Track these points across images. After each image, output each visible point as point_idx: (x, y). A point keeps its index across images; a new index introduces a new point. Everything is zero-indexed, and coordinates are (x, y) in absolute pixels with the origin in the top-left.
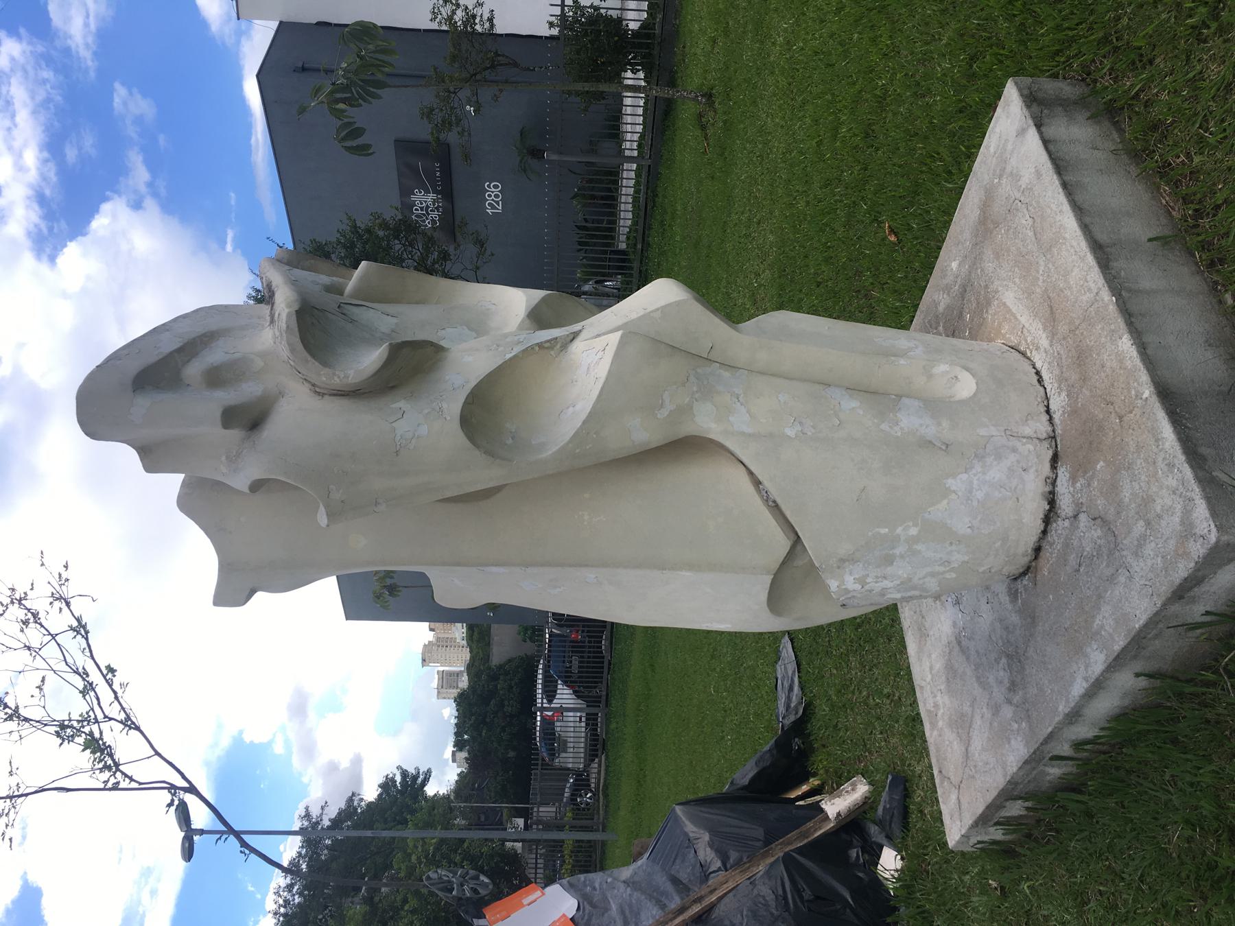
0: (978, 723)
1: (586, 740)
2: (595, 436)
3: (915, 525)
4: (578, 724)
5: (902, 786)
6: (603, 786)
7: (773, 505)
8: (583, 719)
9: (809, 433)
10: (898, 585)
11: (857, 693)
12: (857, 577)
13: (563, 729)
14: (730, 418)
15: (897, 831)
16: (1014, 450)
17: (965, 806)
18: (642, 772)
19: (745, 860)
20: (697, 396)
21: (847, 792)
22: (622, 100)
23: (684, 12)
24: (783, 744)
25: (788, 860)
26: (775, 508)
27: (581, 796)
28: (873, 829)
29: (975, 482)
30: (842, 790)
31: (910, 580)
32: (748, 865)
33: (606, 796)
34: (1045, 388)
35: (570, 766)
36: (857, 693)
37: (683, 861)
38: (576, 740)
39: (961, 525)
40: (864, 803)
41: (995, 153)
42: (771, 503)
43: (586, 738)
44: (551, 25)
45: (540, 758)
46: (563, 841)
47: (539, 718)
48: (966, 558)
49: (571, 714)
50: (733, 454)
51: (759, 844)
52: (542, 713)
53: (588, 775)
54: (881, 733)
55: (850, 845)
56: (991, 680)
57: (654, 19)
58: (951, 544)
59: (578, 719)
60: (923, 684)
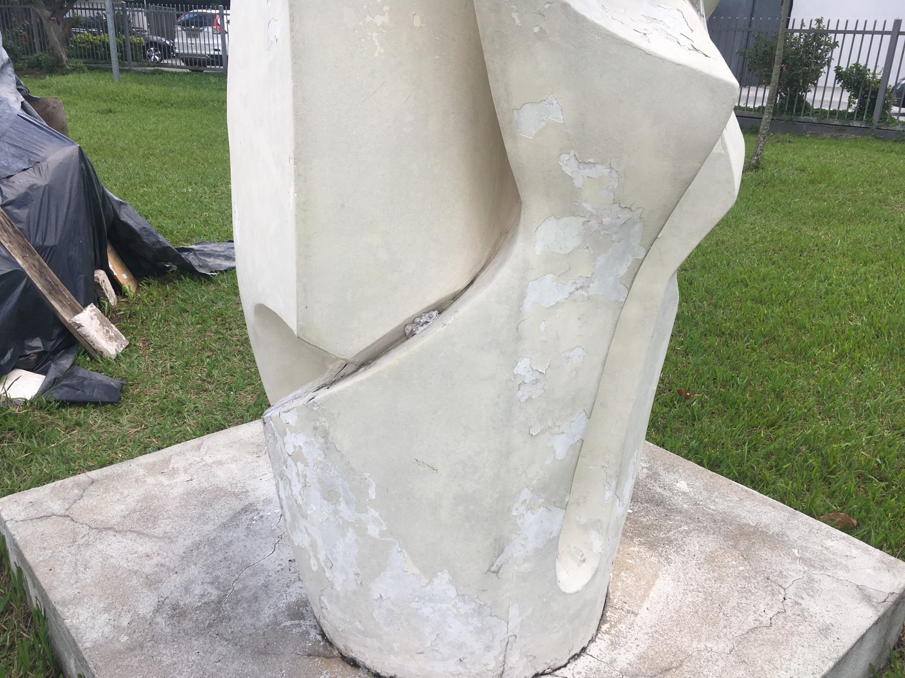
0: (141, 549)
1: (199, 55)
2: (536, 30)
3: (382, 534)
4: (212, 48)
5: (107, 399)
6: (162, 70)
7: (407, 332)
8: (216, 53)
9: (519, 394)
10: (296, 501)
11: (216, 337)
12: (303, 451)
13: (206, 34)
14: (550, 277)
15: (58, 394)
16: (488, 648)
17: (42, 527)
18: (170, 105)
19: (17, 226)
20: (594, 223)
21: (108, 331)
22: (755, 85)
23: (817, 141)
24: (165, 253)
25: (18, 275)
26: (403, 335)
27: (156, 51)
28: (66, 362)
29: (444, 606)
30: (109, 326)
31: (305, 517)
32: (11, 230)
33: (154, 73)
34: (565, 666)
35: (176, 40)
36: (216, 337)
37: (13, 156)
38: (198, 46)
39: (381, 587)
40: (96, 351)
41: (827, 548)
42: (409, 328)
43: (201, 55)
44: (819, 21)
45: (180, 12)
46: (107, 32)
47: (213, 11)
48: (338, 588)
49: (220, 42)
50: (483, 269)
51: (39, 240)
52: (218, 14)
53: (174, 57)
54: (172, 367)
55: (45, 339)
56: (194, 571)
57: (813, 115)
58: (357, 574)
59: (216, 48)
60: (203, 451)
